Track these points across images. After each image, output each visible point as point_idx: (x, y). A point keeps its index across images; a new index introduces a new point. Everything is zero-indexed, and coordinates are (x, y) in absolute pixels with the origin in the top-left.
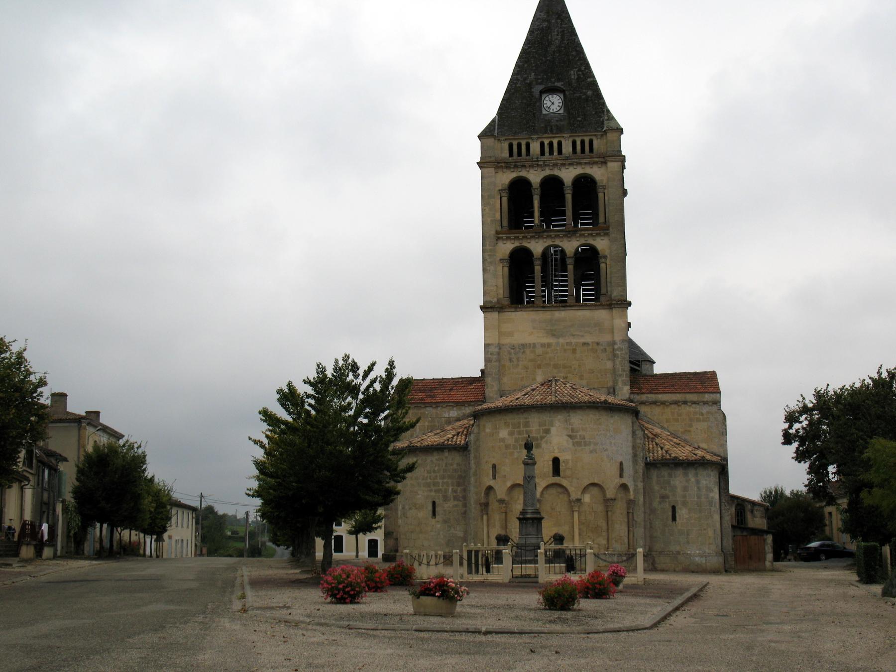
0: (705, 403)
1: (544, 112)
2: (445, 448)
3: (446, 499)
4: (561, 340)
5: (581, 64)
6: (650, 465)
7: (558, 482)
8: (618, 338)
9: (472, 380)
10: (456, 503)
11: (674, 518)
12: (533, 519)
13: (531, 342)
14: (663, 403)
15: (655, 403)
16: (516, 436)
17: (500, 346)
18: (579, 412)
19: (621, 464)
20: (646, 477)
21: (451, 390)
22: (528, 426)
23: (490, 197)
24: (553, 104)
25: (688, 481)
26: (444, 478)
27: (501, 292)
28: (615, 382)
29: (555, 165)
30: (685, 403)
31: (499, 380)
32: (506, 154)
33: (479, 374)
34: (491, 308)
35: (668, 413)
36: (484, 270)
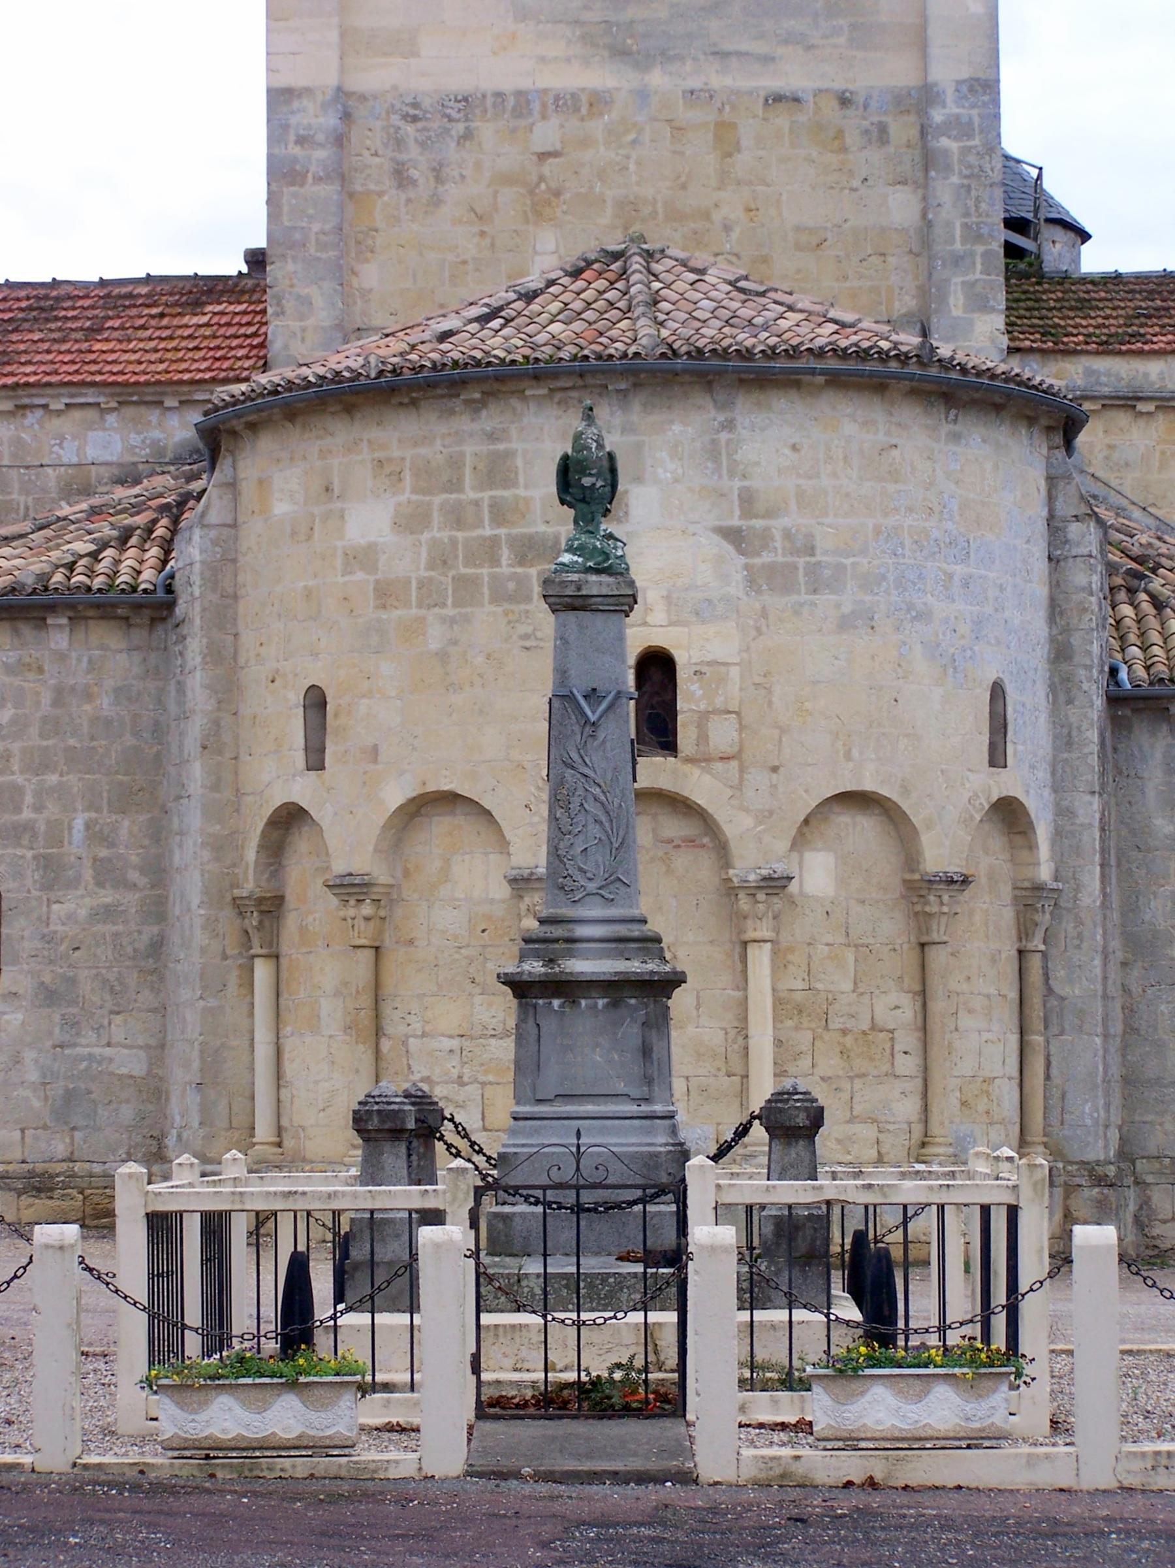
2: (52, 608)
4: (657, 79)
8: (946, 72)
9: (201, 291)
10: (107, 897)
12: (615, 988)
13: (507, 84)
16: (437, 532)
19: (997, 692)
20: (1117, 769)
21: (92, 332)
22: (509, 482)
26: (45, 766)
31: (342, 274)
33: (233, 265)
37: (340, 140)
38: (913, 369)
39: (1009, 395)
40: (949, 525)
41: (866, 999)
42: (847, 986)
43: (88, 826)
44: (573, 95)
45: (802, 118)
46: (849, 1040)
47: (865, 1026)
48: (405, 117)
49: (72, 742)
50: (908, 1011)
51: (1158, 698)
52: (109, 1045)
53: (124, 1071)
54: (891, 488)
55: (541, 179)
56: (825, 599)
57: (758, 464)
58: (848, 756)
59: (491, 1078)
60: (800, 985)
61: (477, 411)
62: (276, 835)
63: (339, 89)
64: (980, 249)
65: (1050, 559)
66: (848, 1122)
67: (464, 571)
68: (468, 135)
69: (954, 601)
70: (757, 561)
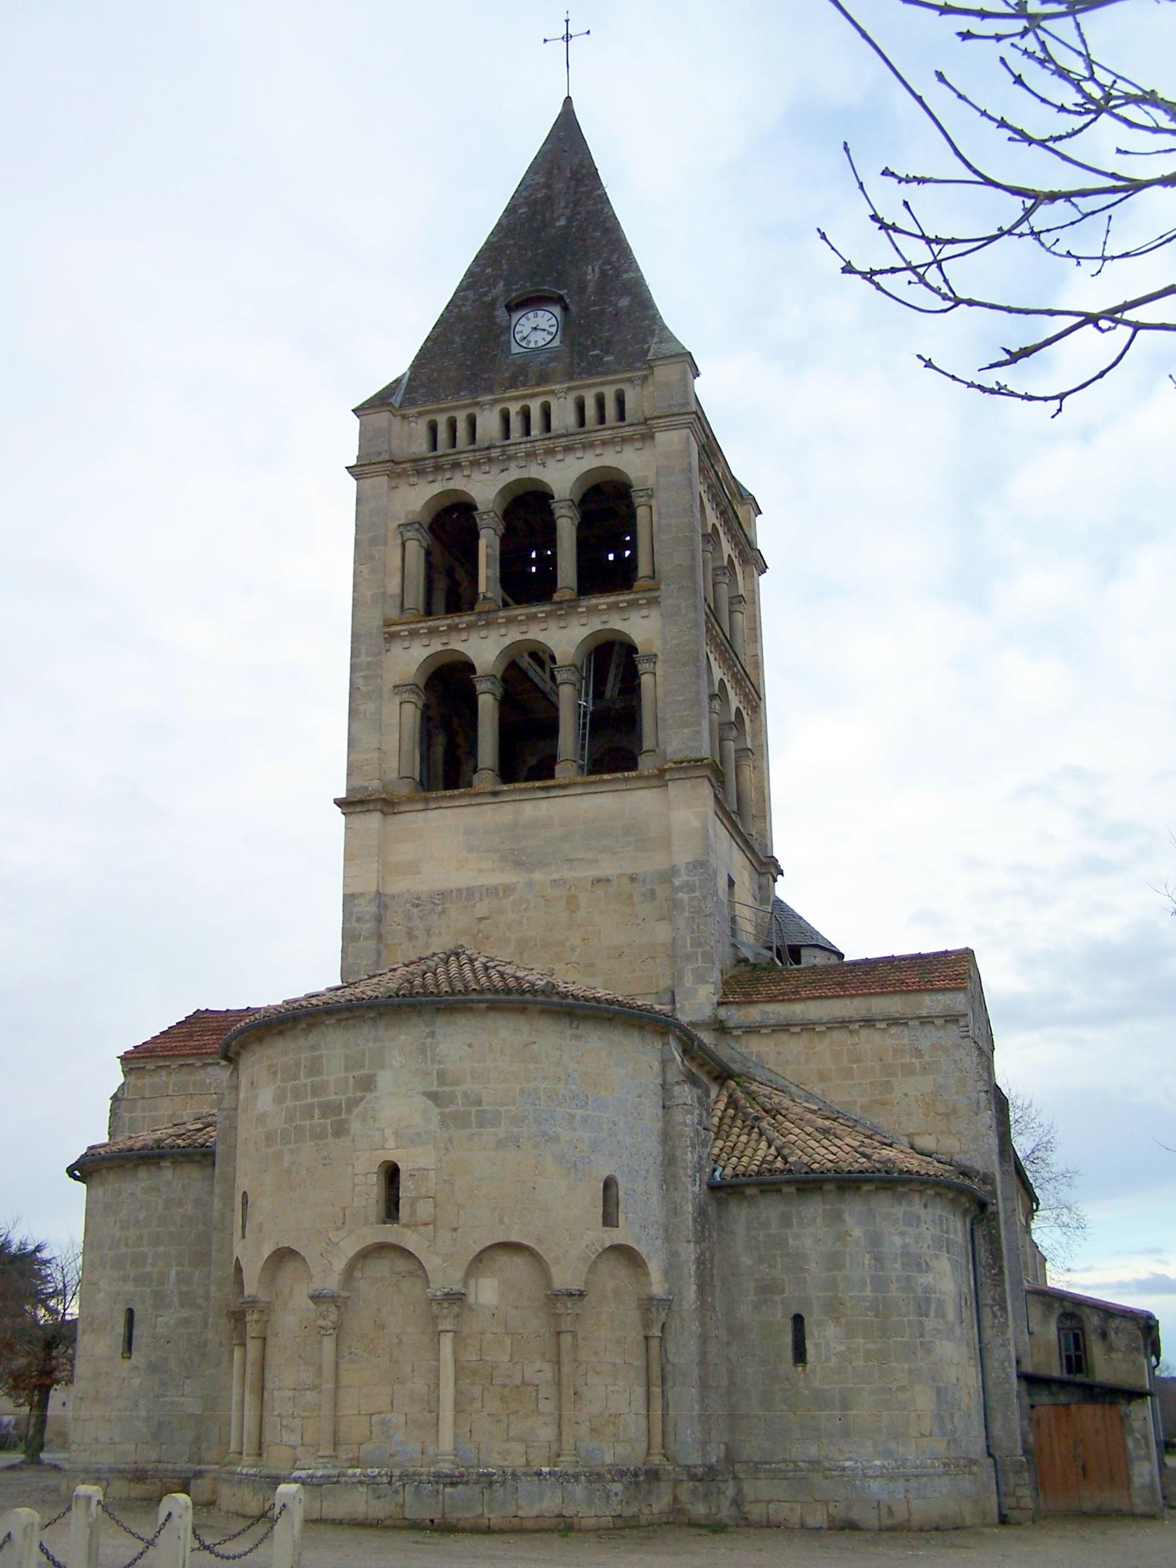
0: (926, 1021)
1: (515, 349)
2: (161, 1157)
3: (160, 1300)
4: (537, 876)
5: (612, 252)
6: (723, 1191)
7: (391, 1239)
10: (186, 1313)
11: (800, 1355)
13: (463, 885)
14: (808, 1027)
15: (784, 1027)
16: (289, 1103)
17: (381, 899)
18: (462, 1020)
19: (609, 1185)
20: (706, 1224)
23: (373, 542)
24: (537, 329)
25: (843, 1236)
27: (393, 763)
28: (678, 976)
29: (531, 455)
30: (868, 1022)
32: (420, 446)
34: (362, 802)
35: (824, 1051)
36: (353, 713)
37: (379, 919)
38: (540, 998)
39: (616, 1013)
40: (573, 1087)
41: (519, 1367)
42: (506, 1358)
43: (177, 1274)
44: (496, 887)
45: (611, 890)
46: (506, 1391)
47: (518, 1382)
48: (413, 905)
49: (172, 1229)
50: (548, 1373)
51: (738, 1185)
52: (182, 1395)
53: (190, 1410)
54: (532, 1066)
55: (479, 931)
56: (487, 1130)
57: (448, 1055)
58: (501, 1222)
59: (306, 1414)
60: (474, 1358)
61: (307, 1035)
62: (1142, 1323)
63: (379, 894)
64: (700, 950)
65: (664, 1107)
66: (505, 1441)
67: (299, 1123)
68: (443, 912)
69: (575, 1130)
70: (447, 1110)
